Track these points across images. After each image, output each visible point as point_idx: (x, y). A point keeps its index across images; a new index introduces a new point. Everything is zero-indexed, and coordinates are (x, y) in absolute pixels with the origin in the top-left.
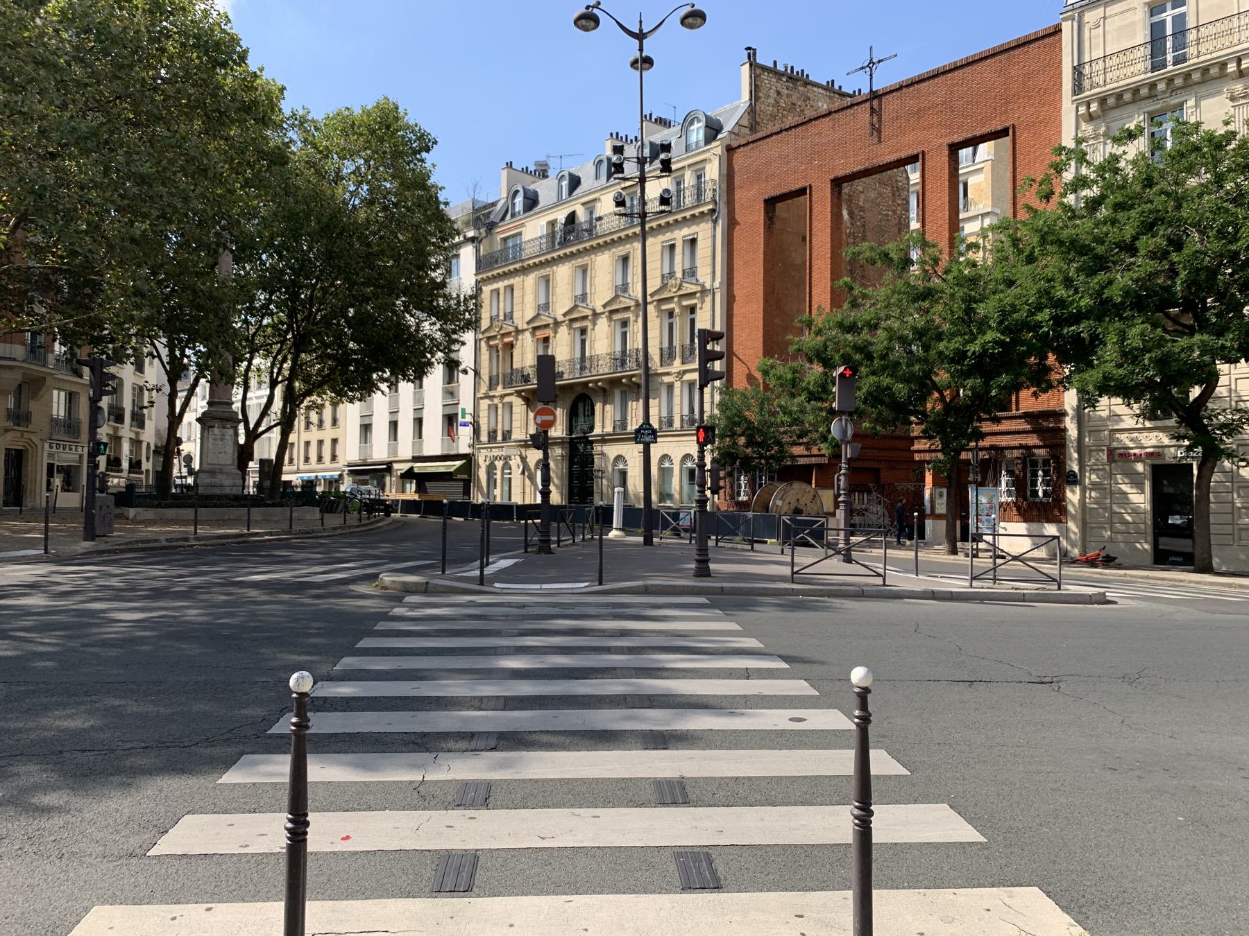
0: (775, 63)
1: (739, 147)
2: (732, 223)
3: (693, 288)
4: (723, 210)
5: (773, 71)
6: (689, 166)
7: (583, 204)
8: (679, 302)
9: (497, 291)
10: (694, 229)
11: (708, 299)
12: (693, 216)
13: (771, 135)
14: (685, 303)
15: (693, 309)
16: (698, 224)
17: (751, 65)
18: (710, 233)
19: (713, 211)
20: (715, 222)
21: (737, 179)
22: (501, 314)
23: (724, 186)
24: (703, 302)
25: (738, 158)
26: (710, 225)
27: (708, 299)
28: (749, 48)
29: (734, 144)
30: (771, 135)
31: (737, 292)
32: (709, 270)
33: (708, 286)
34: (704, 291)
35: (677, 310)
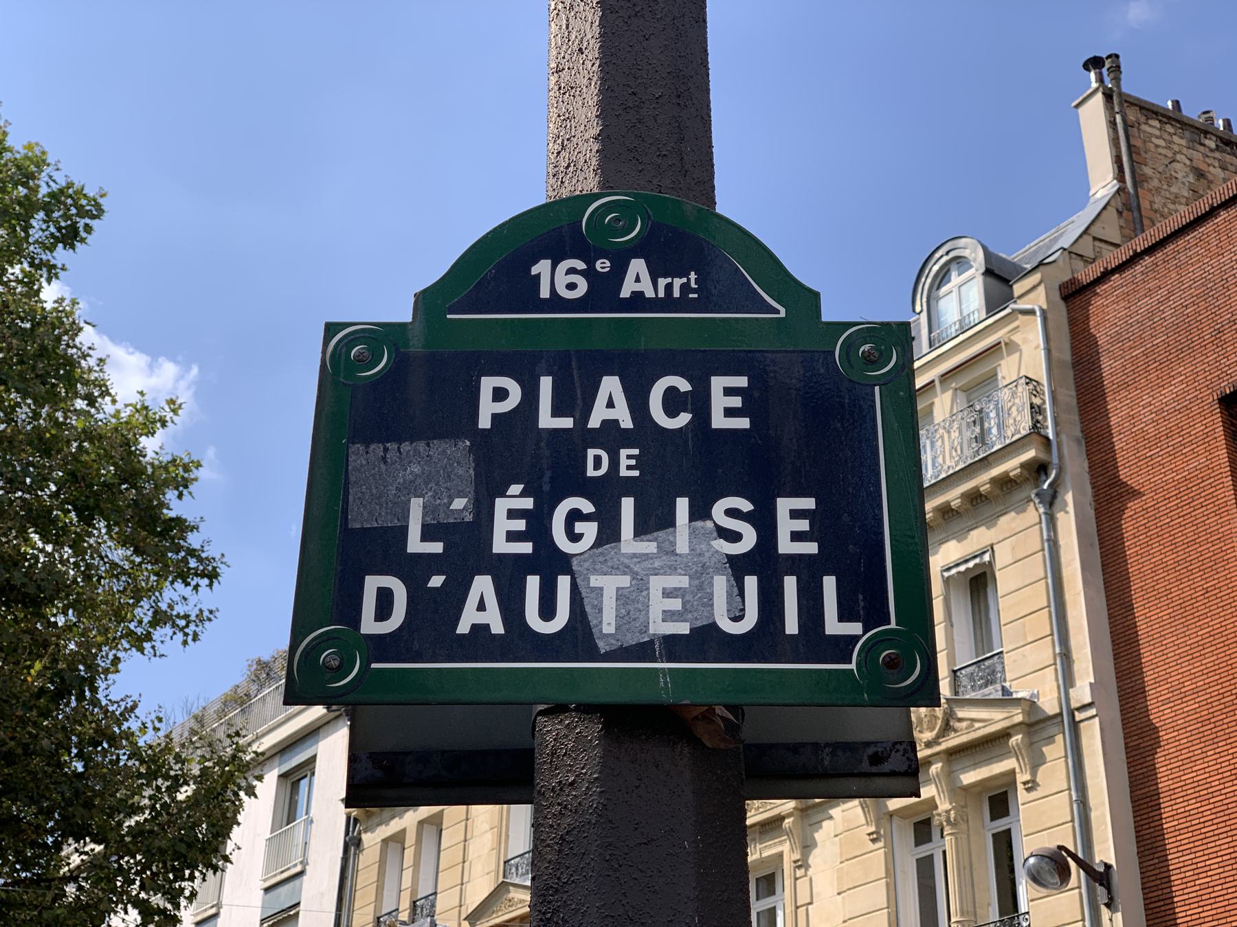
0: (1176, 104)
1: (1106, 275)
2: (1109, 498)
3: (997, 719)
4: (1075, 463)
5: (1173, 118)
6: (945, 377)
7: (758, 899)
8: (950, 775)
9: (398, 838)
10: (979, 538)
11: (1056, 751)
12: (975, 498)
13: (1212, 212)
14: (969, 778)
15: (1000, 801)
16: (990, 522)
17: (1108, 96)
18: (1034, 540)
19: (1038, 469)
20: (1051, 500)
21: (1109, 366)
22: (405, 904)
23: (1069, 395)
24: (1037, 762)
25: (1108, 313)
26: (1033, 513)
27: (1056, 751)
28: (1094, 63)
29: (1087, 274)
30: (1212, 212)
31: (1160, 711)
32: (1046, 652)
33: (1049, 704)
34: (1037, 725)
35: (944, 805)
